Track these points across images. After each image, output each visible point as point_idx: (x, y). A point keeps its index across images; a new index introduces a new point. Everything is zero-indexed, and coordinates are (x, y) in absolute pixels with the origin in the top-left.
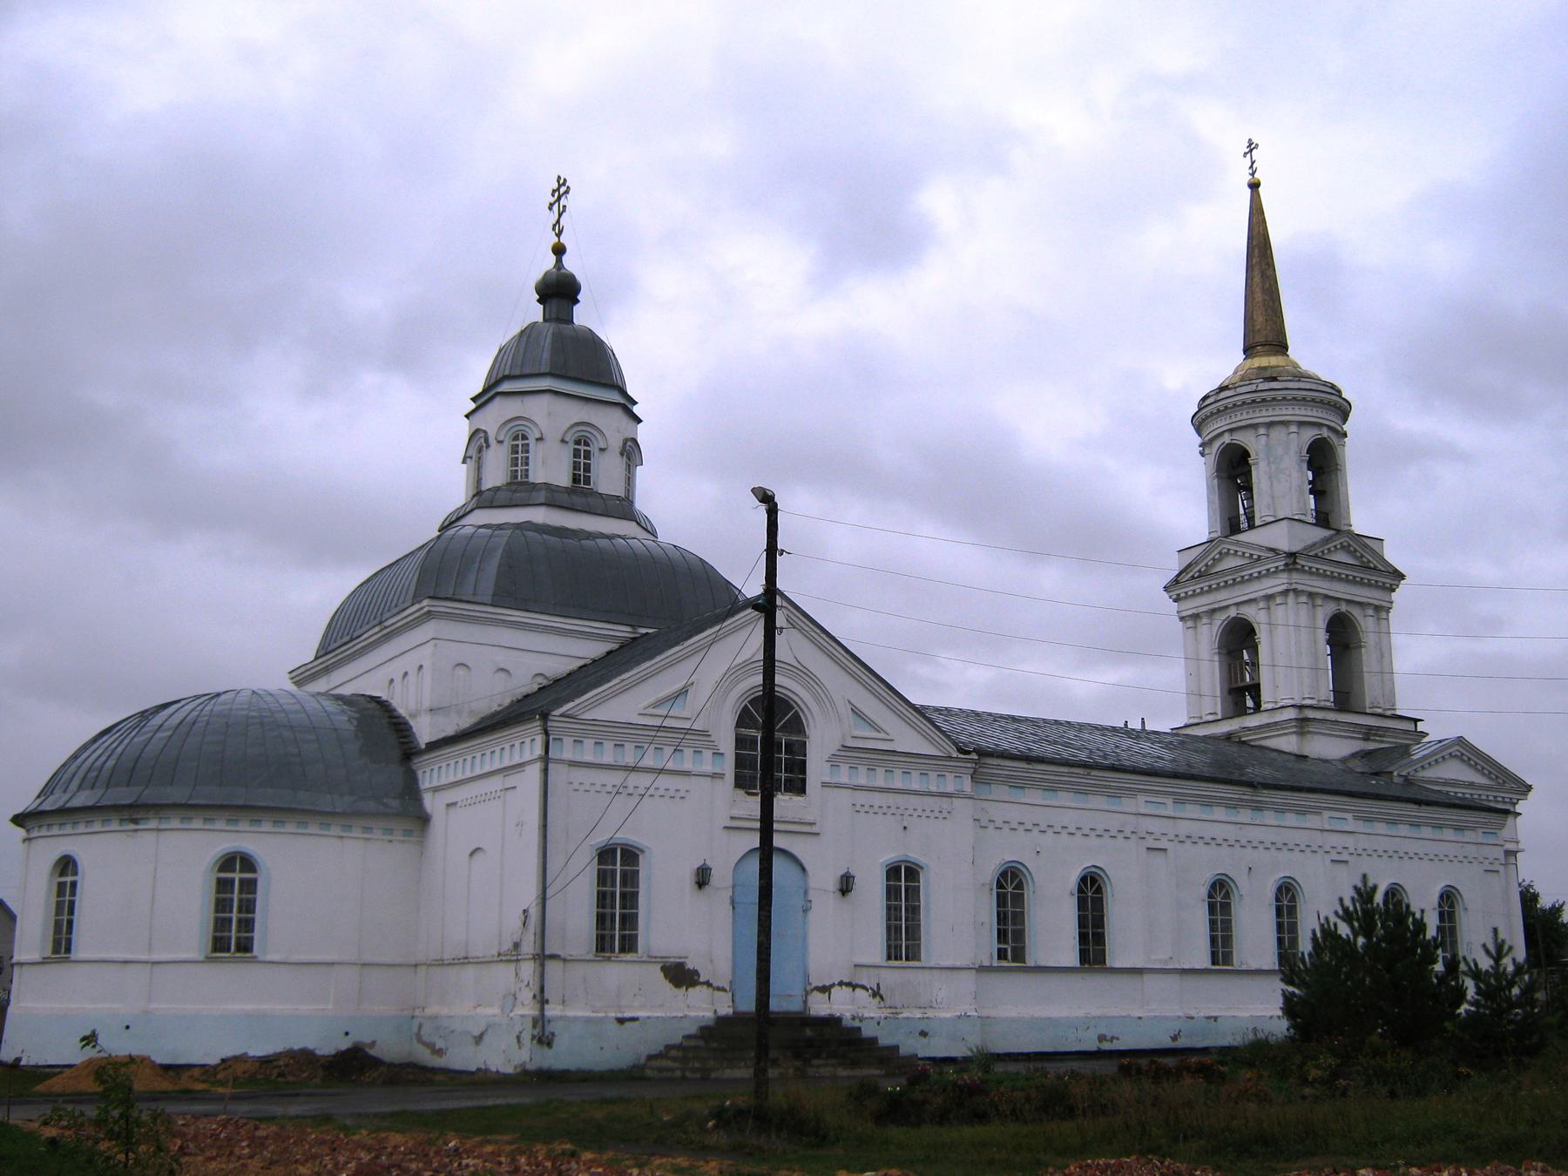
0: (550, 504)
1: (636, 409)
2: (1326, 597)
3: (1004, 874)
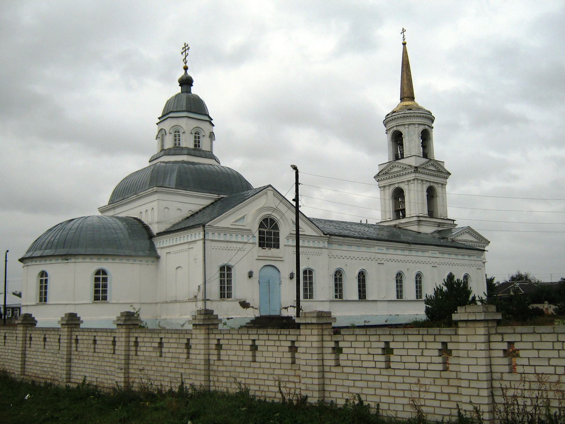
0: (188, 154)
1: (212, 121)
2: (427, 181)
3: (336, 272)
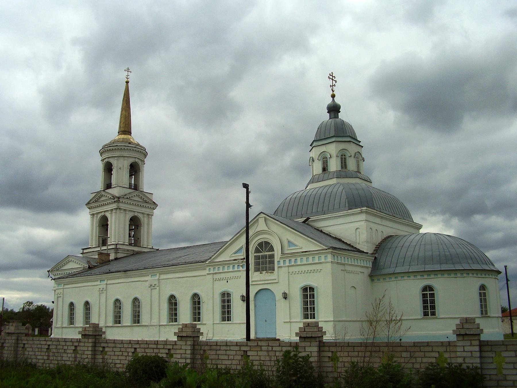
1: (360, 144)
